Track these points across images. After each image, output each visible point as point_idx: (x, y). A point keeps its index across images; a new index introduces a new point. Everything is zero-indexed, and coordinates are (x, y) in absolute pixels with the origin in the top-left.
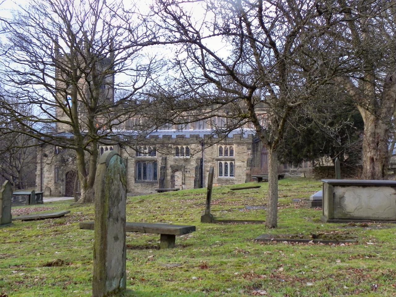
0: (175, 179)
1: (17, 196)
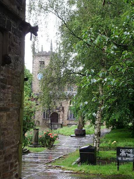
1: (54, 125)
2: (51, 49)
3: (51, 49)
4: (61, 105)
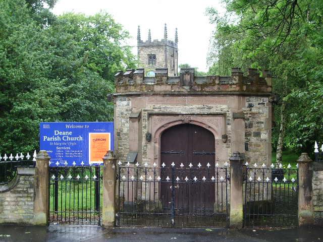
2: (166, 36)
3: (166, 36)
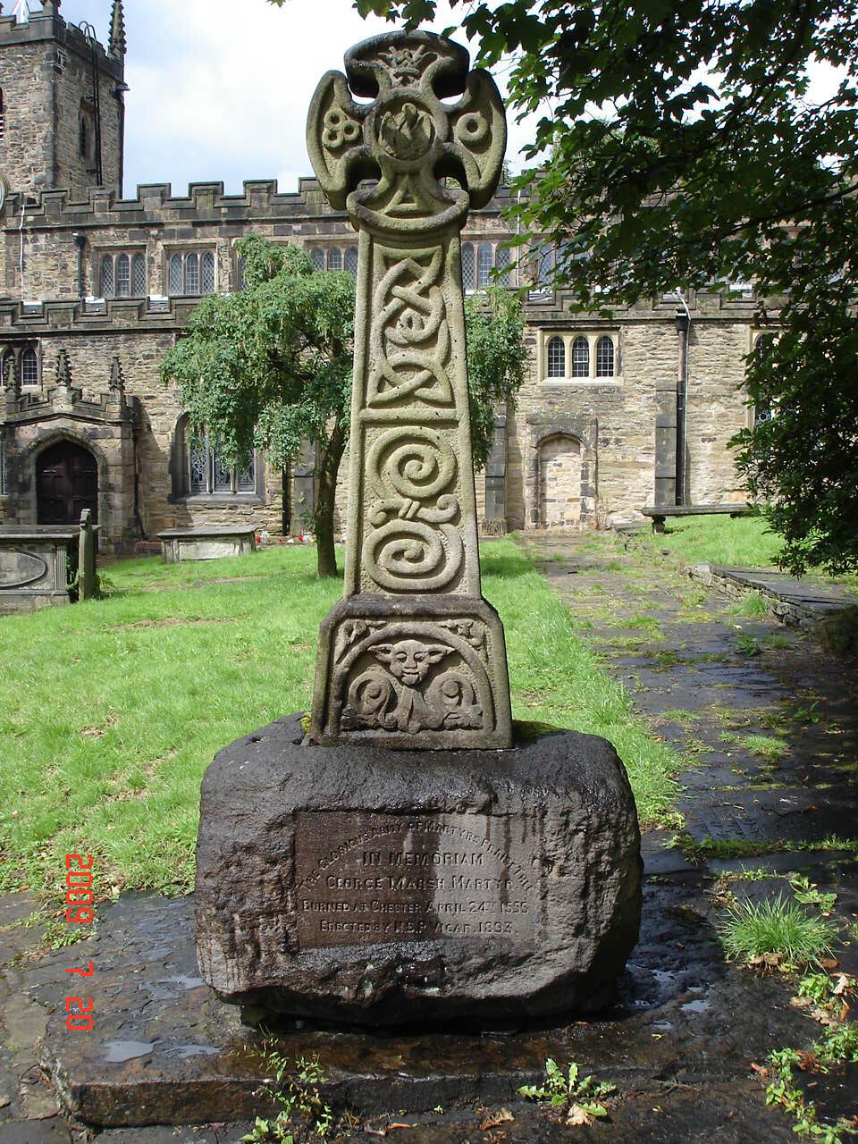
0: (549, 475)
4: (117, 384)
